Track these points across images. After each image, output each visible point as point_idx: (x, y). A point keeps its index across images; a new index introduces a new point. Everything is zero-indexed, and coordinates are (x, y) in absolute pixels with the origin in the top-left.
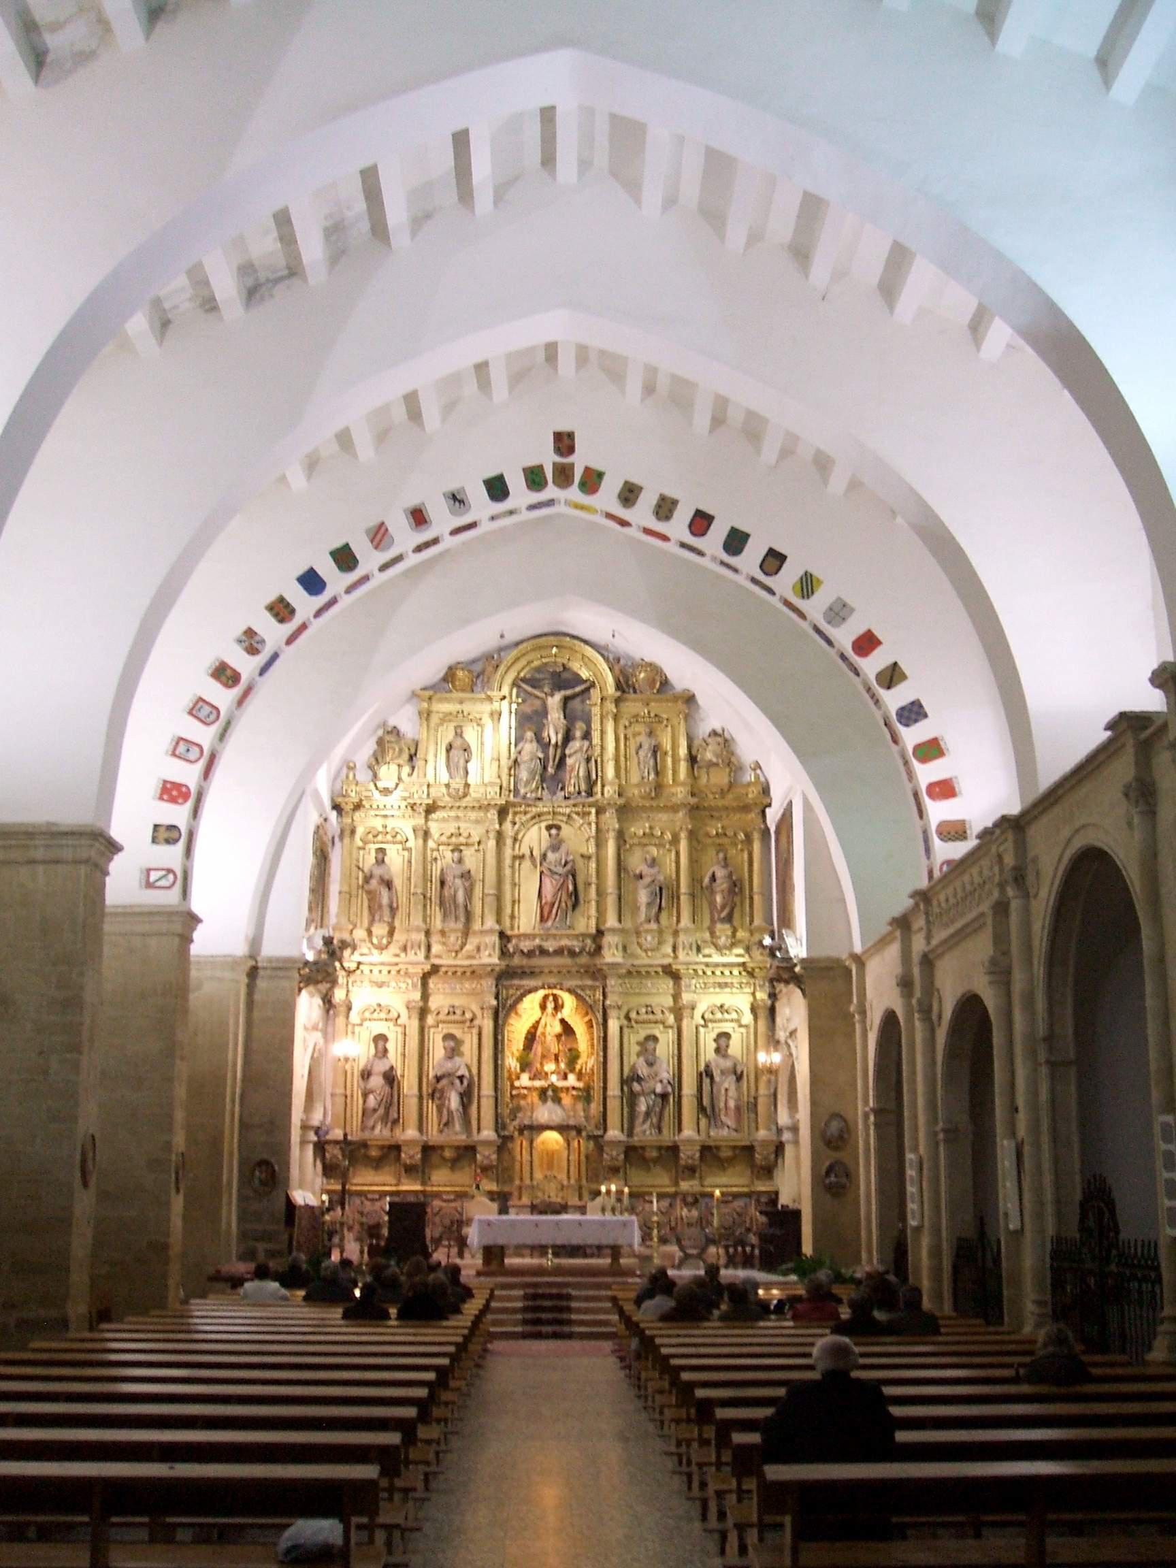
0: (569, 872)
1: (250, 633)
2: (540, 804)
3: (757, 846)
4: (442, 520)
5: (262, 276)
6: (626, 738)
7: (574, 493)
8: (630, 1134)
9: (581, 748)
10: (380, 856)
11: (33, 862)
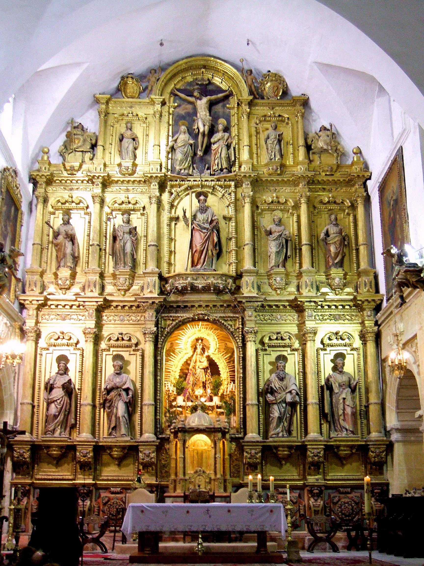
0: (214, 227)
3: (360, 210)
8: (266, 435)
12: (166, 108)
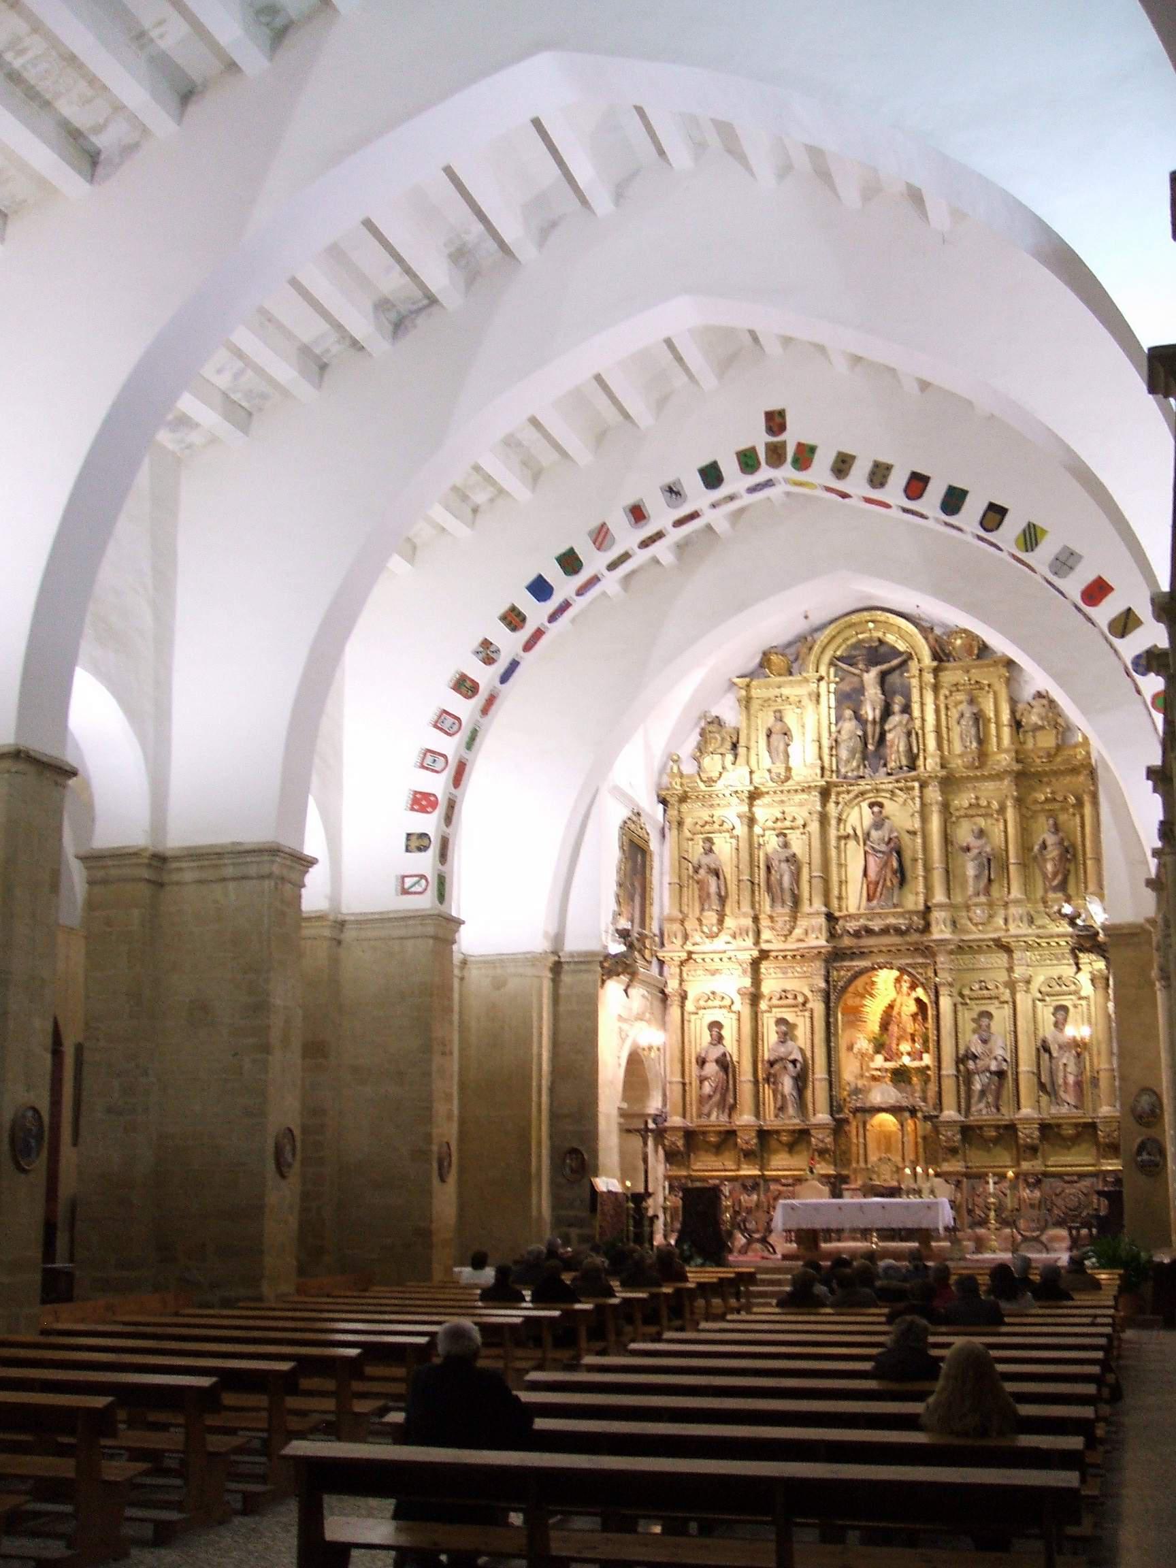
0: (892, 849)
1: (486, 644)
2: (862, 782)
4: (661, 516)
5: (404, 308)
6: (947, 708)
7: (787, 471)
9: (901, 722)
10: (707, 845)
11: (224, 880)
12: (823, 684)
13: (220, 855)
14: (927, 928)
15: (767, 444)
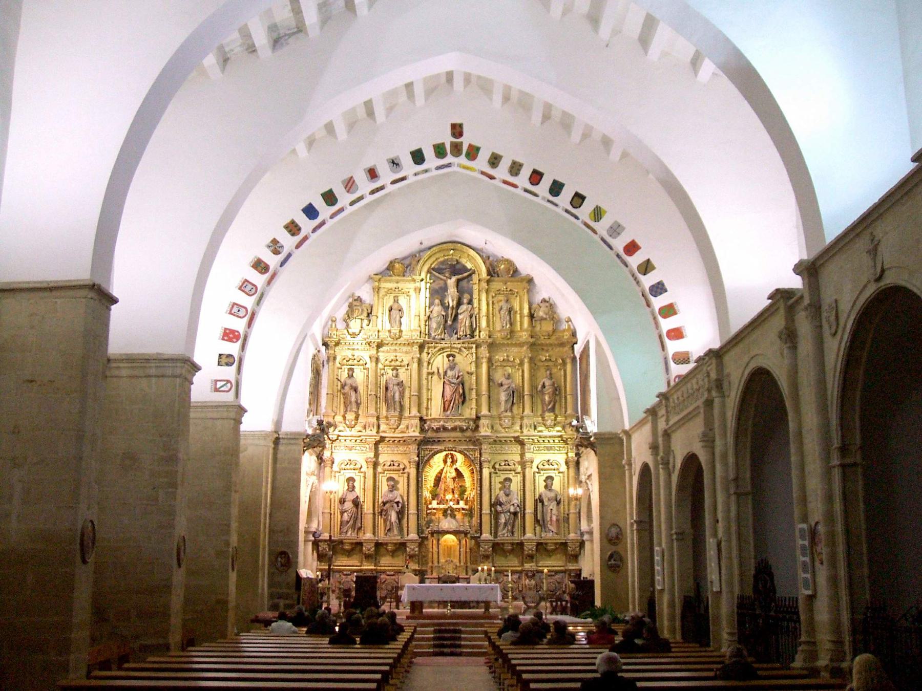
1: (275, 242)
2: (443, 342)
3: (569, 367)
4: (386, 176)
5: (282, 32)
6: (493, 303)
7: (463, 160)
8: (496, 536)
13: (147, 360)
14: (477, 427)
15: (443, 144)
